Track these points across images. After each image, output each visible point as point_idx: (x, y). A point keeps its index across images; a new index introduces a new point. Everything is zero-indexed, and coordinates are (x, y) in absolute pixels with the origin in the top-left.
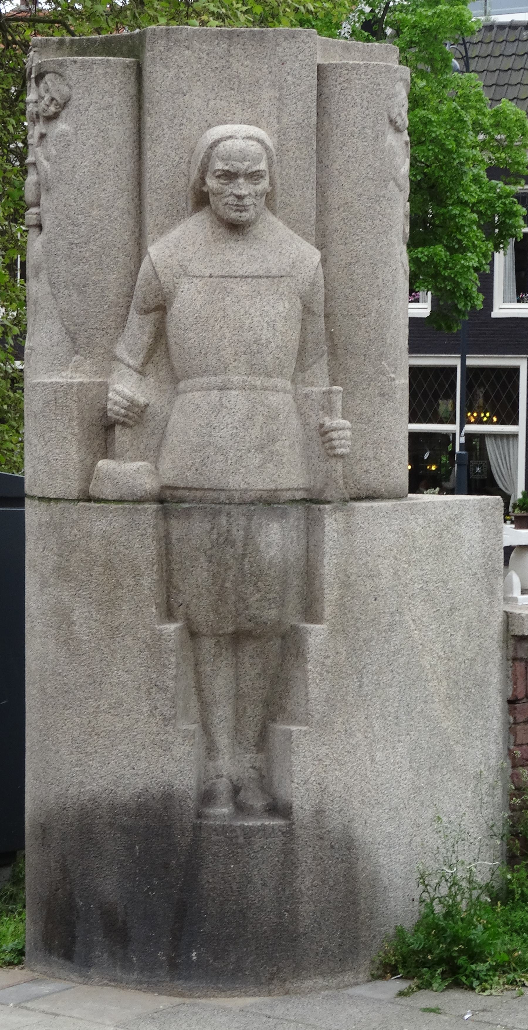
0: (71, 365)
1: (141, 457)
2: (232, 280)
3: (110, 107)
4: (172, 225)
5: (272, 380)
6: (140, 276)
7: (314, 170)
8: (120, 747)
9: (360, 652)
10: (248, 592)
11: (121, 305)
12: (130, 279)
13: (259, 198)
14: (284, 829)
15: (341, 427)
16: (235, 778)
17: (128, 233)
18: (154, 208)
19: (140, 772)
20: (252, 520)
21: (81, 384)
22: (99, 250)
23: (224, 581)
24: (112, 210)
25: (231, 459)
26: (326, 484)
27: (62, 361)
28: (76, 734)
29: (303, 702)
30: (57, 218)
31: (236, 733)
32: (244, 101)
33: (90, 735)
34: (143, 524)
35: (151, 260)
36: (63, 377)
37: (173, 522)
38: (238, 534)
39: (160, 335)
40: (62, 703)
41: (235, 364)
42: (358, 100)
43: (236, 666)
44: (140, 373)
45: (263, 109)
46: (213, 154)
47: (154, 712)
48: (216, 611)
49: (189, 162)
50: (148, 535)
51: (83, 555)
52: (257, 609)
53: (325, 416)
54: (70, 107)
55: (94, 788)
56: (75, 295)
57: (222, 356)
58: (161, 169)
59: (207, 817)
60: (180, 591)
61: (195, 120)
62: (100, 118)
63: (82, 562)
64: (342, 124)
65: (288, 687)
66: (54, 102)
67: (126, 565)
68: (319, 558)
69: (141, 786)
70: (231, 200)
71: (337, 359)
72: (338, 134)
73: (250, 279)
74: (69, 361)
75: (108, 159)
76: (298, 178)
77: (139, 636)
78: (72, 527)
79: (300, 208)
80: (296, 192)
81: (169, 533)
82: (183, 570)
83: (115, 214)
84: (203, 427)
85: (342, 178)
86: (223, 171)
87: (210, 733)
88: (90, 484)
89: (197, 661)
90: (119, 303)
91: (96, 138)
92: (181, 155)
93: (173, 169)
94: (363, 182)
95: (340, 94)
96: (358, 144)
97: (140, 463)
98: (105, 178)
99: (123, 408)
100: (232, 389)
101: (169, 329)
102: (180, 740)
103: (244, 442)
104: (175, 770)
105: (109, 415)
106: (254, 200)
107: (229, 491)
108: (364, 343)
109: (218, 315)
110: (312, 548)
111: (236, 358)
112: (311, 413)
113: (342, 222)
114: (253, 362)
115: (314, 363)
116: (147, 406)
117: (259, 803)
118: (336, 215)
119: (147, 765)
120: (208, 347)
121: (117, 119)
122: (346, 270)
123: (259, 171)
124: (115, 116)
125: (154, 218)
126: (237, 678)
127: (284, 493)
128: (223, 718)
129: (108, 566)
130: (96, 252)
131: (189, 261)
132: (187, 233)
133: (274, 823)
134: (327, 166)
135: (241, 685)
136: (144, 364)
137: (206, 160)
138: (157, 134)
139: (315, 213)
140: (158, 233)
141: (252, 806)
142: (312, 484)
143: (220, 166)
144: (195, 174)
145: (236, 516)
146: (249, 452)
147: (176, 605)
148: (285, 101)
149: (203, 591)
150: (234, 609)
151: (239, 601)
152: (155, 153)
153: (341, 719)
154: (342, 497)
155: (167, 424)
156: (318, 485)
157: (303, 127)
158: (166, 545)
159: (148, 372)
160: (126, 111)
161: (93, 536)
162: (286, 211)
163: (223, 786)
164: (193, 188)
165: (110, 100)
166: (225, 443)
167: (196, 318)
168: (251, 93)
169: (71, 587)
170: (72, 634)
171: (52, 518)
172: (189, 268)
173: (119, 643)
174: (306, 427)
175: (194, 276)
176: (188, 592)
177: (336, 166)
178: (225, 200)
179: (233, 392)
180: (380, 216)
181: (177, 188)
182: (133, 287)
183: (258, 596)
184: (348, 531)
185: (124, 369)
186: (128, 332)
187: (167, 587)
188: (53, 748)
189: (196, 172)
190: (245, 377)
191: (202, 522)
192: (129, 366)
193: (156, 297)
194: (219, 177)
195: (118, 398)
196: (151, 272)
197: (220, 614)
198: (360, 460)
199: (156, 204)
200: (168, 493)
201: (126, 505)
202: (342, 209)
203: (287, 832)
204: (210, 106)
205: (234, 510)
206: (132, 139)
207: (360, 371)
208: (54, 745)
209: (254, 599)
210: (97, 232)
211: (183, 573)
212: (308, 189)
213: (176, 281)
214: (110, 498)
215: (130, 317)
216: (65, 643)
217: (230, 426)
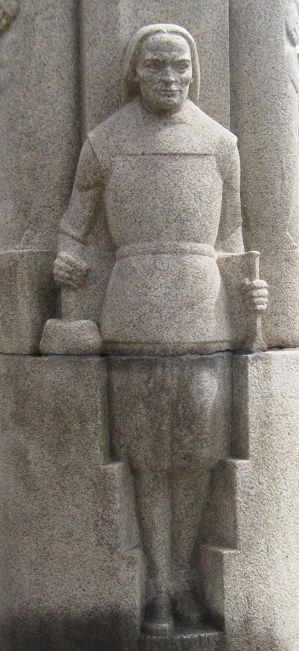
0: (23, 239)
1: (85, 315)
2: (162, 157)
3: (52, 17)
4: (108, 115)
5: (200, 245)
6: (81, 158)
7: (228, 69)
8: (72, 572)
9: (278, 481)
10: (183, 434)
11: (65, 185)
12: (72, 163)
13: (184, 85)
14: (218, 639)
15: (260, 286)
16: (173, 593)
17: (70, 125)
18: (92, 100)
19: (90, 594)
20: (184, 369)
21: (31, 253)
22: (45, 138)
23: (160, 425)
24: (56, 104)
25: (165, 316)
26: (247, 336)
27: (16, 235)
28: (34, 557)
29: (232, 528)
30: (9, 113)
31: (172, 552)
32: (168, 10)
33: (46, 560)
34: (87, 375)
35: (90, 142)
36: (16, 249)
37: (114, 373)
38: (171, 382)
39: (98, 209)
40: (22, 530)
41: (166, 231)
42: (262, 14)
43: (172, 497)
44: (83, 243)
45: (184, 17)
46: (143, 47)
47: (101, 542)
48: (153, 450)
49: (122, 61)
50: (92, 385)
51: (36, 404)
52: (191, 448)
53: (245, 277)
54: (19, 19)
55: (51, 605)
56: (26, 178)
57: (155, 224)
58: (98, 67)
59: (150, 632)
60: (121, 434)
61: (126, 26)
62: (44, 27)
63: (35, 409)
64: (250, 33)
65: (218, 514)
66: (6, 16)
67: (73, 411)
68: (243, 401)
69: (91, 605)
70: (159, 86)
71: (249, 230)
72: (247, 42)
73: (178, 156)
74: (21, 236)
75: (52, 61)
76: (215, 75)
77: (86, 475)
78: (25, 379)
79: (217, 101)
80: (213, 88)
81: (110, 383)
82: (123, 415)
83: (59, 108)
84: (139, 287)
85: (251, 78)
86: (153, 60)
87: (150, 554)
88: (40, 341)
89: (138, 493)
90: (63, 184)
91: (42, 43)
92: (115, 56)
93: (108, 67)
94: (268, 82)
95: (247, 8)
96: (264, 50)
97: (84, 321)
98: (49, 77)
99: (67, 272)
100: (164, 253)
101: (107, 202)
102: (124, 566)
103: (176, 300)
104: (121, 592)
105: (55, 279)
106: (180, 87)
107: (164, 344)
108: (272, 216)
109: (151, 188)
110: (236, 392)
111: (168, 225)
112: (233, 275)
113: (252, 115)
114: (183, 229)
115: (232, 232)
116: (88, 271)
117: (194, 616)
118: (246, 109)
119: (96, 587)
120: (142, 216)
121: (59, 28)
122: (255, 155)
123: (184, 60)
124: (57, 24)
125: (92, 109)
126: (173, 507)
127: (212, 345)
128: (161, 542)
129: (57, 413)
130: (43, 141)
131: (123, 141)
132: (121, 119)
133: (209, 634)
134: (237, 69)
135: (176, 513)
136: (86, 235)
137: (137, 52)
138: (92, 38)
139: (229, 106)
140: (96, 122)
141: (189, 617)
142: (234, 336)
143: (149, 56)
144: (127, 66)
145: (170, 367)
146: (181, 309)
147: (118, 446)
148: (203, 11)
149: (142, 434)
150: (169, 448)
151: (174, 441)
152: (92, 55)
153: (263, 540)
154: (261, 347)
155: (107, 286)
156: (240, 336)
157: (218, 33)
158: (108, 388)
159: (89, 242)
160: (67, 22)
161: (44, 386)
162: (206, 103)
163: (163, 601)
164: (126, 80)
165: (53, 11)
166: (159, 301)
167: (131, 191)
168: (173, 5)
169: (26, 431)
170: (28, 471)
171: (9, 370)
172: (124, 147)
173: (68, 480)
174: (228, 287)
175: (128, 155)
176: (128, 434)
177: (245, 68)
178: (155, 87)
179: (166, 256)
180: (282, 111)
181: (111, 83)
182: (74, 170)
183: (191, 437)
184: (267, 375)
185: (69, 241)
186: (72, 209)
187: (110, 430)
188: (15, 566)
189: (128, 65)
190: (176, 242)
191: (140, 372)
192: (73, 237)
193: (95, 174)
194: (148, 66)
195: (62, 264)
196: (90, 153)
197: (158, 453)
198: (271, 316)
199: (94, 97)
200: (109, 347)
201: (73, 358)
202: (251, 104)
203: (220, 641)
204: (139, 15)
205: (168, 362)
206: (71, 46)
207: (269, 240)
208: (16, 564)
209: (187, 440)
210: (43, 123)
211: (124, 418)
212: (223, 85)
213: (112, 159)
214: (58, 353)
215: (73, 195)
216: (23, 478)
217: (164, 286)
